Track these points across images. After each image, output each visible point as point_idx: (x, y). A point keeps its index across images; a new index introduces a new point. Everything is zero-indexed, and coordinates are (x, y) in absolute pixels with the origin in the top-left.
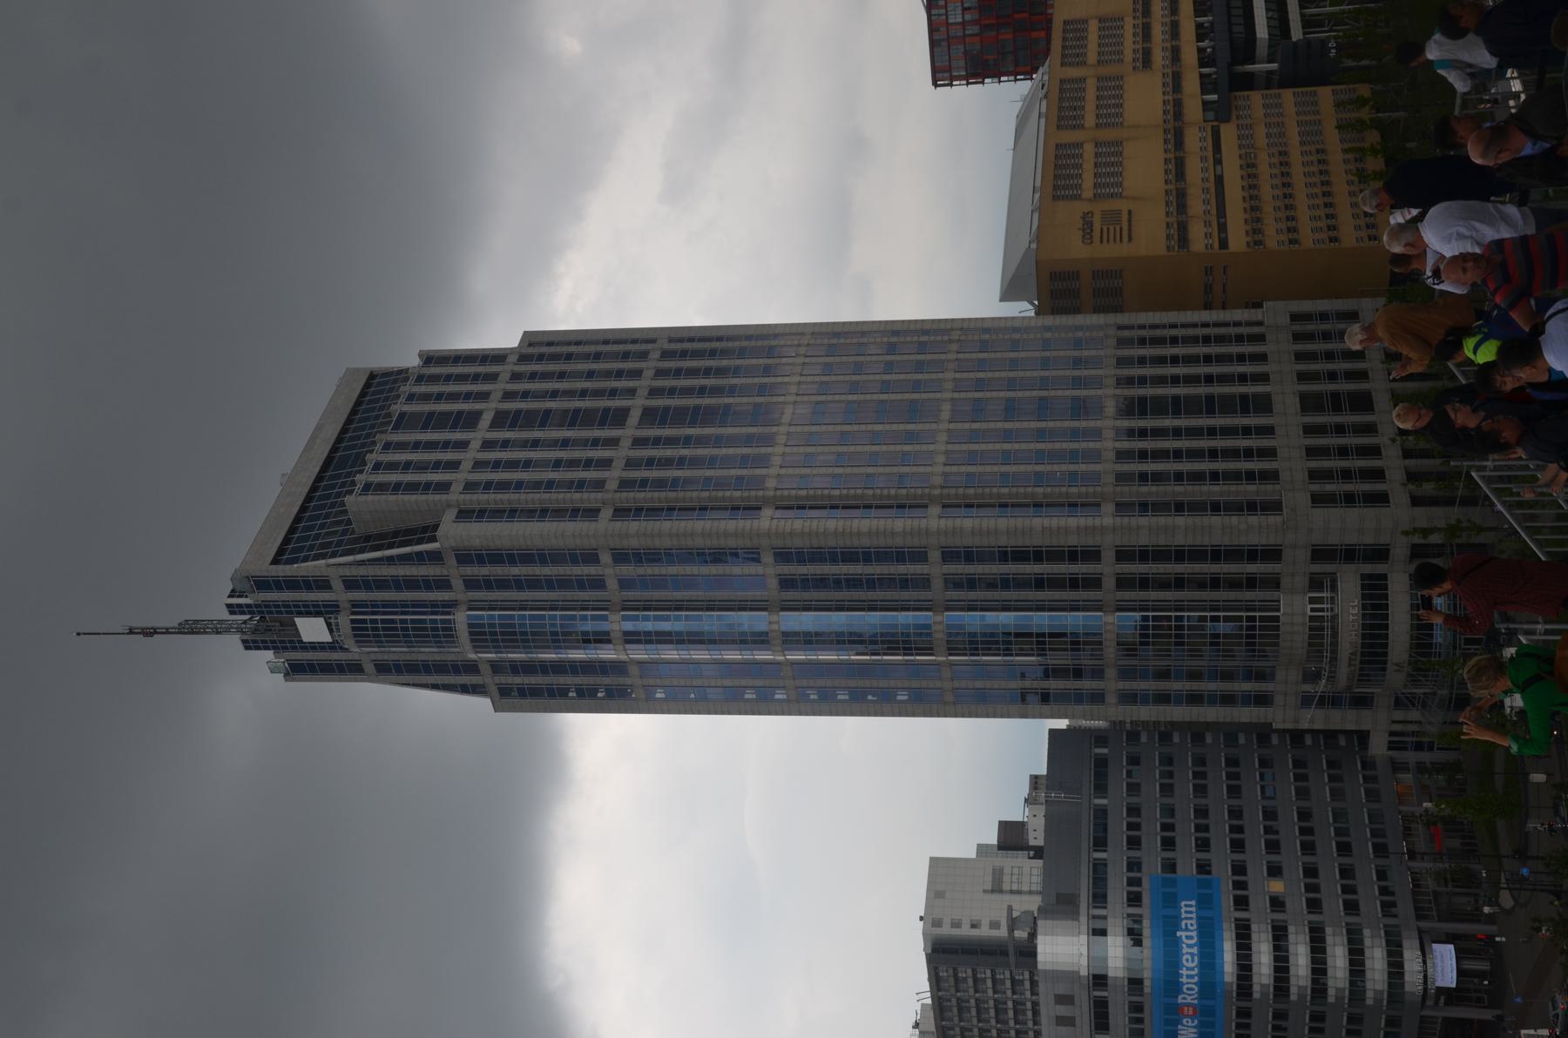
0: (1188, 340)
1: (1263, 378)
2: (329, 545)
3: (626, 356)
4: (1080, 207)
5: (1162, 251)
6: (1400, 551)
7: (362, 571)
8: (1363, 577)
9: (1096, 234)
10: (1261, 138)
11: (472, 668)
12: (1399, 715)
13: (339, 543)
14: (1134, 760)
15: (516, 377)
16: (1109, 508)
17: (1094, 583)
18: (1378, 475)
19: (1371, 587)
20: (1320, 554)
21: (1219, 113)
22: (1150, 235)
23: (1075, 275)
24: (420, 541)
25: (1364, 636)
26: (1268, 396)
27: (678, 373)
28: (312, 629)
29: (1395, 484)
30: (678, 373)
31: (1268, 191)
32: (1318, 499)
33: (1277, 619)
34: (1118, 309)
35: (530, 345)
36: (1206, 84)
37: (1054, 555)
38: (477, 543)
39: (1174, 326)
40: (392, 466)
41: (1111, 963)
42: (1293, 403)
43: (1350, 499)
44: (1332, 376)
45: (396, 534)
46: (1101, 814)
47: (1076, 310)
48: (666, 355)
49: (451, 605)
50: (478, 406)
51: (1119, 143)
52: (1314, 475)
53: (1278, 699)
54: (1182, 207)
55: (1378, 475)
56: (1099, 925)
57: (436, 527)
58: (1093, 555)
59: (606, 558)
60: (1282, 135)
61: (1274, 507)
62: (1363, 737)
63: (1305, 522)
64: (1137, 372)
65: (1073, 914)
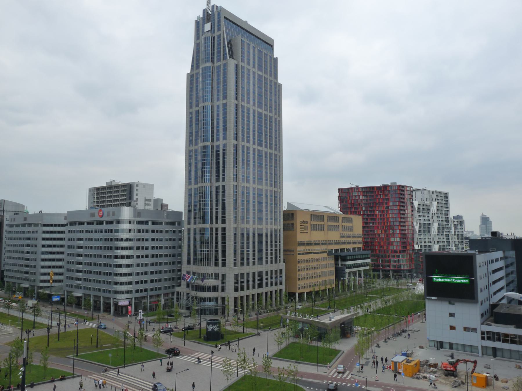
0: (276, 238)
1: (267, 263)
2: (229, 31)
3: (276, 145)
4: (308, 220)
5: (298, 240)
6: (223, 295)
7: (222, 39)
8: (218, 286)
9: (302, 224)
10: (323, 263)
11: (198, 68)
12: (185, 294)
13: (229, 34)
14: (174, 232)
15: (271, 81)
16: (235, 226)
17: (217, 222)
18: (242, 289)
19: (215, 288)
20: (223, 276)
21: (330, 253)
22: (301, 237)
23: (293, 219)
24: (229, 54)
25: (210, 286)
26: (262, 264)
27: (271, 159)
28: (208, 27)
29: (240, 294)
30: (271, 159)
31: (311, 264)
32: (237, 275)
33: (208, 266)
34: (284, 230)
35: (279, 86)
36: (337, 250)
37: (224, 213)
38: (229, 68)
39: (280, 242)
40: (249, 48)
41: (122, 225)
42: (260, 270)
43: (237, 283)
44: (267, 279)
45: (231, 48)
46: (160, 223)
47: (284, 220)
48: (275, 119)
49: (213, 61)
50: (264, 71)
51: (323, 230)
52: (243, 275)
53: (188, 266)
54: (308, 244)
55: (242, 289)
56: (132, 222)
57: (233, 58)
58: (224, 222)
59: (225, 101)
60: (324, 267)
61: (235, 265)
62: (180, 286)
63: (231, 272)
64: (274, 259)
65: (134, 216)
